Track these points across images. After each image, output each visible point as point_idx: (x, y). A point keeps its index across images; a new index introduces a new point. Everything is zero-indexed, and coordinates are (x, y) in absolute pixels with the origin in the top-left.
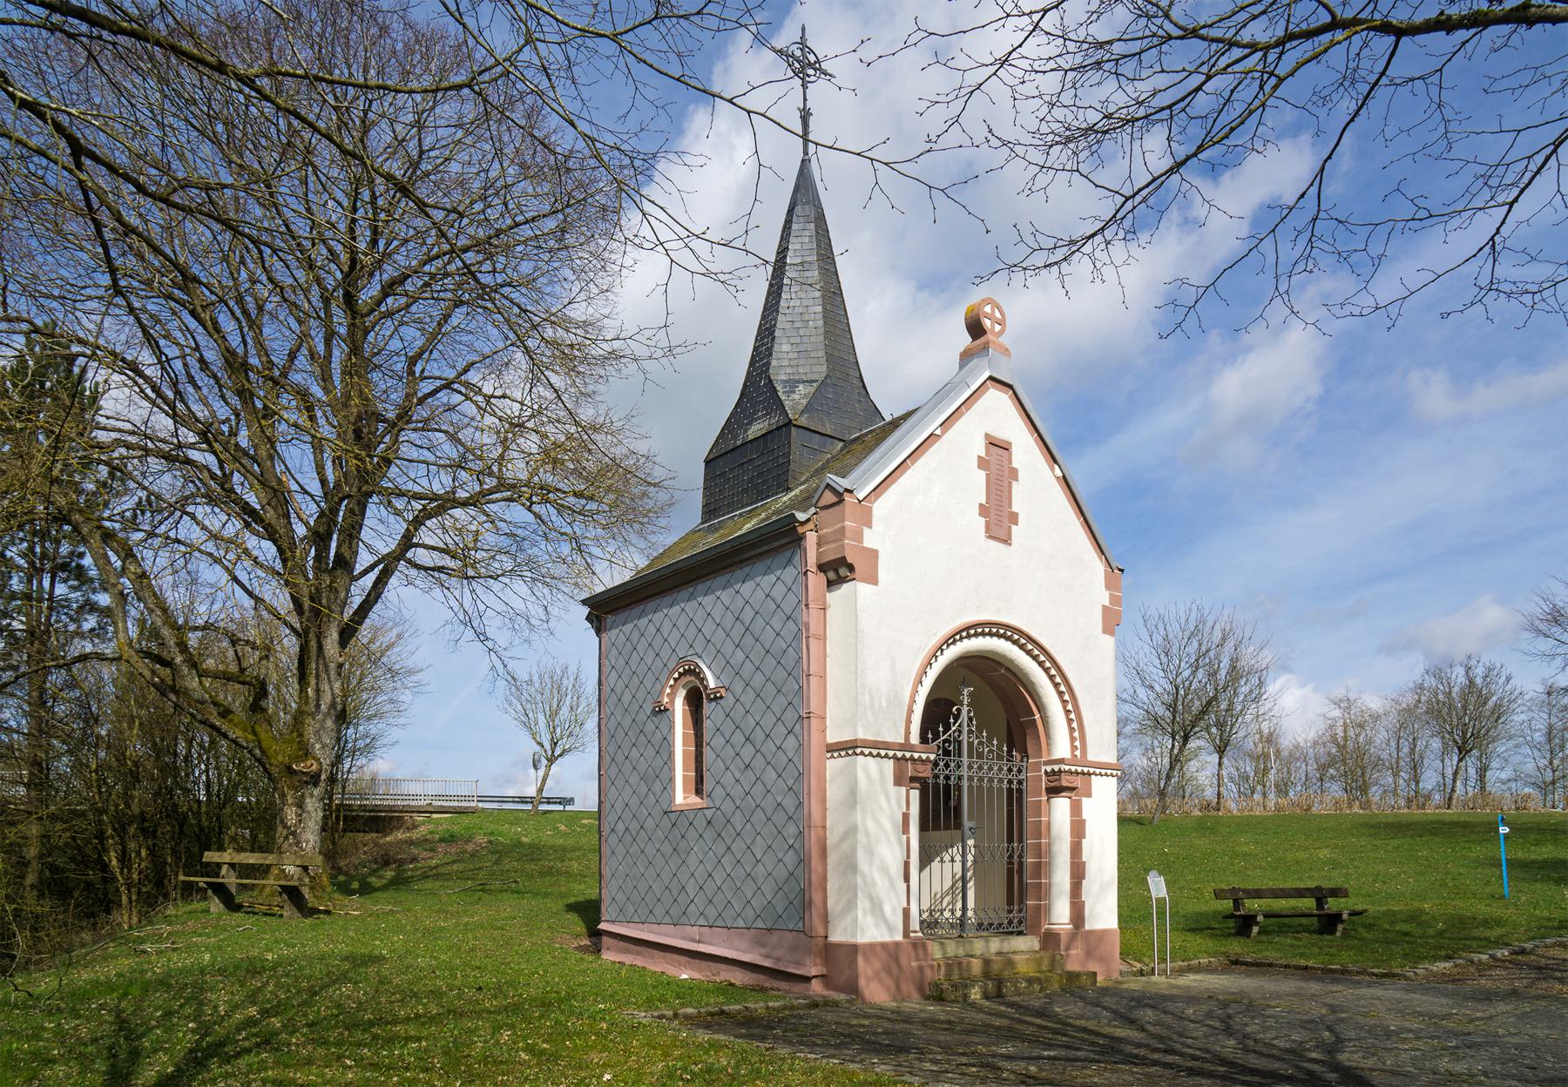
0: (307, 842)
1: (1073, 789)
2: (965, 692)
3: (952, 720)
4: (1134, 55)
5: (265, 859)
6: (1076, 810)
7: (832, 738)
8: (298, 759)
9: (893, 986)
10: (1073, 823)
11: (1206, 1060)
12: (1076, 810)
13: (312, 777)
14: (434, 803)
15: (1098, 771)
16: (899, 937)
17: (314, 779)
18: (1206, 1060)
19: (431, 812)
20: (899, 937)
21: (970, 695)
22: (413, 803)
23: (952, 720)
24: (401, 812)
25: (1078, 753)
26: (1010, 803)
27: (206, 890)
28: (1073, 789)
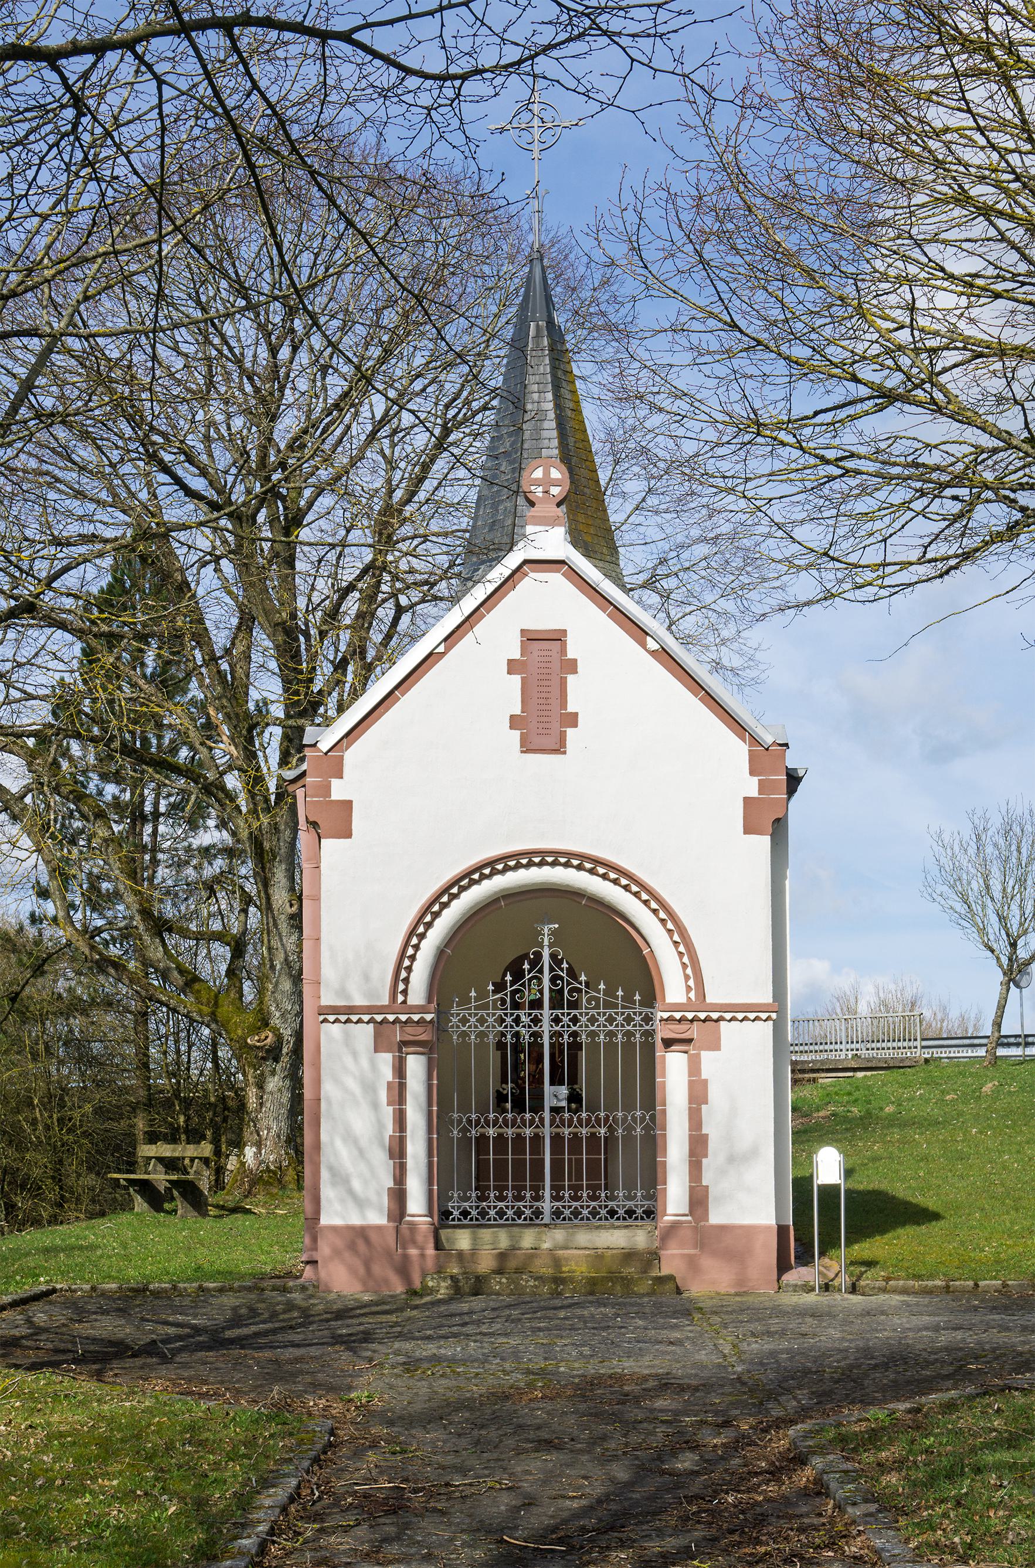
0: (269, 1129)
1: (689, 1041)
2: (546, 931)
3: (526, 966)
4: (431, 13)
5: (174, 1150)
6: (694, 1067)
7: (327, 999)
8: (255, 1030)
9: (362, 1271)
10: (691, 1084)
11: (189, 1336)
12: (694, 1067)
13: (268, 1051)
14: (863, 1053)
15: (728, 1016)
16: (377, 1217)
17: (274, 1053)
18: (257, 1335)
19: (855, 1070)
20: (377, 1217)
21: (553, 933)
22: (832, 1056)
23: (526, 966)
24: (813, 1071)
25: (692, 995)
26: (629, 1063)
27: (126, 1188)
28: (689, 1041)
